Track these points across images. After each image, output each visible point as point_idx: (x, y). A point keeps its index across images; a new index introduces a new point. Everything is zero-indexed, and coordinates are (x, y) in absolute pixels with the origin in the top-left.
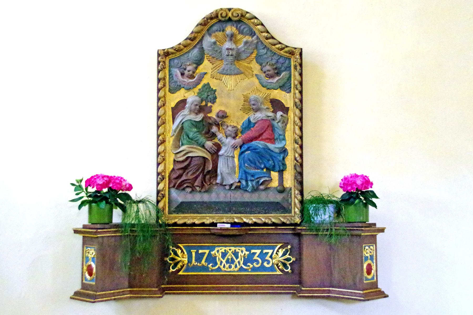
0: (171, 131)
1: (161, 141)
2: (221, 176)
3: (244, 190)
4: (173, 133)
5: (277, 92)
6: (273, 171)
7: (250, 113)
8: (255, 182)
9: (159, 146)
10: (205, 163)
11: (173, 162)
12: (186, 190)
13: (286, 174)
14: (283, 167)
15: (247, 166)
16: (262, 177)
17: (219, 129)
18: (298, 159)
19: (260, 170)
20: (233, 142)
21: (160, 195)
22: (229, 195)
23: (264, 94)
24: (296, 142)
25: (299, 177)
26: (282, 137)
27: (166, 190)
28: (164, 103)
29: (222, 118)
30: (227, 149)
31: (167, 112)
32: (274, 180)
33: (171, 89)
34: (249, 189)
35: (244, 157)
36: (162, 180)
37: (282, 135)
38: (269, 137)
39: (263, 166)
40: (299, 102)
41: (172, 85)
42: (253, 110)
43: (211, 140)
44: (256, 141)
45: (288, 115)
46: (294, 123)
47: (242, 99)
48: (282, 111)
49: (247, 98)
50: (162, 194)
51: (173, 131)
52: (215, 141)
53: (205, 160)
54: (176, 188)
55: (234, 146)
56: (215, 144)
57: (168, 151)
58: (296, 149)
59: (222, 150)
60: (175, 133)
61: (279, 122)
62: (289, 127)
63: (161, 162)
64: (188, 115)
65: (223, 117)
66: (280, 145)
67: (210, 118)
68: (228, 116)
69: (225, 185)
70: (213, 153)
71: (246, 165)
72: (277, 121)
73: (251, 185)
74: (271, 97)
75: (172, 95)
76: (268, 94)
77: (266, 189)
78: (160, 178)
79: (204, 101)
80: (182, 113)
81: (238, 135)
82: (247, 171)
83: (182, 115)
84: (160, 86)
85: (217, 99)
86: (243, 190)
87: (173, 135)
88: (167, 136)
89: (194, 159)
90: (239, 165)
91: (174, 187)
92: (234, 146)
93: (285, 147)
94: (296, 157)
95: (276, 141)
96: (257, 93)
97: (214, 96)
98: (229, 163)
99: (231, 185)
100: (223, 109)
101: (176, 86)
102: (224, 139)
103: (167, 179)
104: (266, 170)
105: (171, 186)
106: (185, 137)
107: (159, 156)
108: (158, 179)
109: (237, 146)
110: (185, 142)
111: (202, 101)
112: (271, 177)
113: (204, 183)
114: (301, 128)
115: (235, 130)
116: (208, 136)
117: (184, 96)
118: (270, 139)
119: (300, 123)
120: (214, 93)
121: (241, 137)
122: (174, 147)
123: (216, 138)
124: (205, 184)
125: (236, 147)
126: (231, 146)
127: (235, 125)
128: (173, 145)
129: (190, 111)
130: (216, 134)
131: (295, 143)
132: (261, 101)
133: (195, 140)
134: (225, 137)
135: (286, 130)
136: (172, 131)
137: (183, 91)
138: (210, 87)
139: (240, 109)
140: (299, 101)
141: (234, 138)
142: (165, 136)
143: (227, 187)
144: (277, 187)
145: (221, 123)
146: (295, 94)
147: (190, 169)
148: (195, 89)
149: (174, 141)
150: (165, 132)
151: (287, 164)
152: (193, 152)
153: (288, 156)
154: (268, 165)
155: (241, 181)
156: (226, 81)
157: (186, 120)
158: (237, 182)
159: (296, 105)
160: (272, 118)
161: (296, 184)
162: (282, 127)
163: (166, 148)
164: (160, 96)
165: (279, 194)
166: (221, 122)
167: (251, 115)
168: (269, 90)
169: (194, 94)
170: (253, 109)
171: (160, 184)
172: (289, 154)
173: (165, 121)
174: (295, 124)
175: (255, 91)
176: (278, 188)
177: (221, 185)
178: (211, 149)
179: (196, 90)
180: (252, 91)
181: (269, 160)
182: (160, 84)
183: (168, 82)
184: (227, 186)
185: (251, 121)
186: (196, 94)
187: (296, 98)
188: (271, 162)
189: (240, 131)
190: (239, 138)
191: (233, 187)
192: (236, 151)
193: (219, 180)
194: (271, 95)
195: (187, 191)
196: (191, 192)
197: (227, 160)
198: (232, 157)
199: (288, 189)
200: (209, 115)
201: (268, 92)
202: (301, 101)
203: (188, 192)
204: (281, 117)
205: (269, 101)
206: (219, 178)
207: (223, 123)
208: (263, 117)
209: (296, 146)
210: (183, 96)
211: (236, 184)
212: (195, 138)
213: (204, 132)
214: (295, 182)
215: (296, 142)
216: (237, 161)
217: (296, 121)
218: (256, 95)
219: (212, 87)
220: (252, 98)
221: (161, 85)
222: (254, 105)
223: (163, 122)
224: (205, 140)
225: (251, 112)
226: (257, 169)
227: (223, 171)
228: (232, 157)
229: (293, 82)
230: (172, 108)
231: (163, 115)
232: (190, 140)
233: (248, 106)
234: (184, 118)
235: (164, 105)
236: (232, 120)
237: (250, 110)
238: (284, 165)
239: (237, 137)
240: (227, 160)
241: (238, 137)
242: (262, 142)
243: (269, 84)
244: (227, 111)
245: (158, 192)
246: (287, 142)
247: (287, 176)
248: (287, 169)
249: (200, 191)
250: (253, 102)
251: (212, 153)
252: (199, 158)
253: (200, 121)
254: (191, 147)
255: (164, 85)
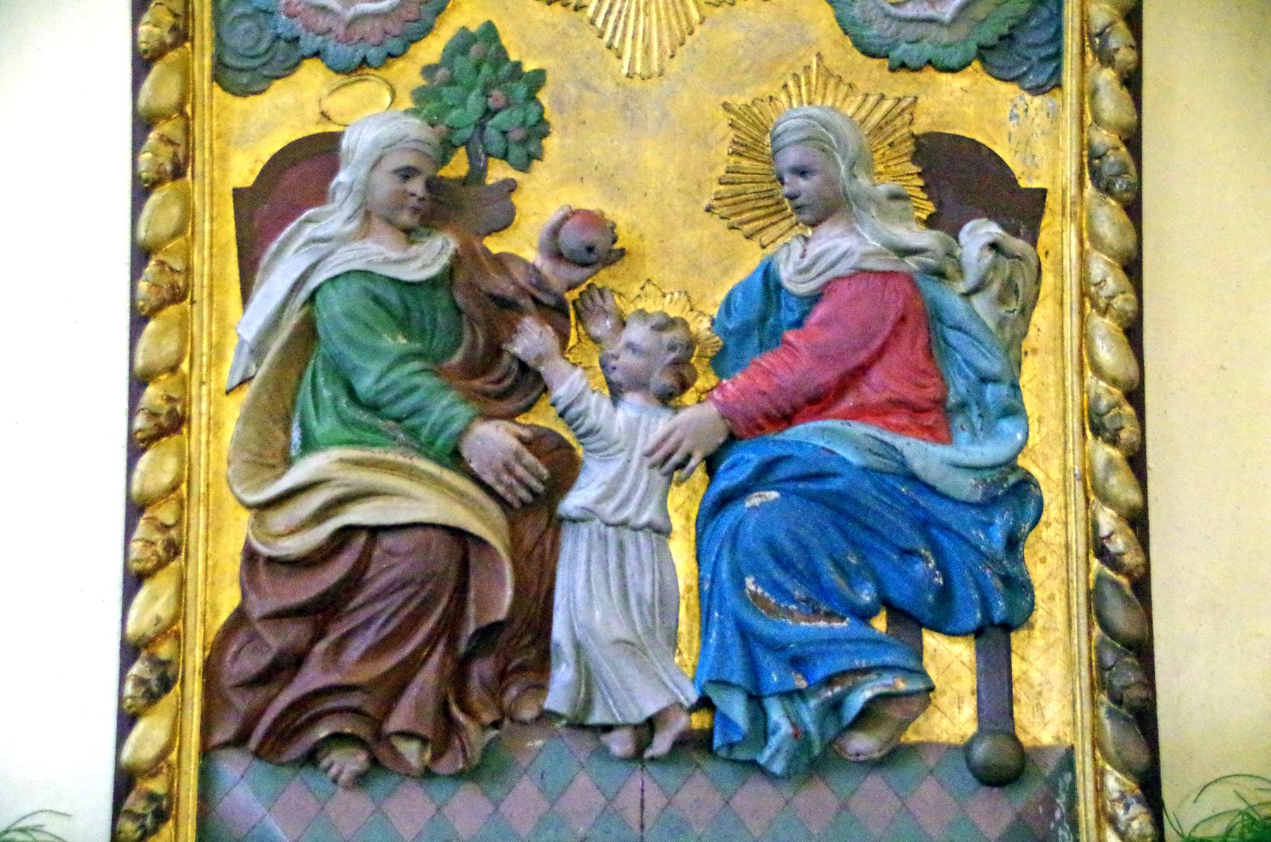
0: (231, 354)
1: (153, 415)
2: (578, 662)
3: (735, 761)
4: (246, 370)
5: (965, 91)
6: (937, 628)
7: (774, 231)
8: (813, 703)
9: (144, 450)
10: (464, 568)
11: (237, 569)
12: (325, 763)
13: (1032, 654)
14: (1010, 605)
15: (760, 591)
16: (866, 671)
17: (564, 338)
18: (1118, 544)
19: (845, 624)
20: (661, 424)
21: (134, 802)
22: (629, 798)
23: (868, 105)
24: (1097, 425)
25: (1128, 676)
26: (991, 393)
27: (184, 767)
28: (181, 156)
29: (584, 265)
30: (620, 477)
31: (198, 220)
32: (944, 692)
33: (228, 59)
34: (774, 756)
35: (734, 536)
36: (152, 698)
37: (996, 380)
38: (912, 395)
39: (866, 596)
40: (1123, 149)
41: (241, 36)
42: (798, 209)
43: (510, 417)
44: (820, 423)
45: (1039, 245)
46: (1083, 294)
47: (723, 134)
48: (993, 216)
49: (755, 133)
50: (152, 797)
51: (246, 349)
52: (541, 423)
53: (466, 553)
54: (261, 745)
55: (668, 456)
56: (538, 442)
57: (203, 490)
58: (1100, 474)
59: (582, 479)
60: (258, 366)
61: (976, 290)
62: (1044, 328)
63: (149, 565)
64: (344, 240)
65: (594, 257)
66: (989, 452)
67: (500, 261)
68: (622, 253)
69: (608, 728)
70: (523, 503)
71: (753, 588)
72: (962, 287)
73: (785, 728)
74: (922, 125)
75: (239, 104)
76: (899, 100)
77: (895, 755)
78: (141, 682)
79: (462, 150)
80: (309, 231)
81: (695, 378)
82: (761, 625)
83: (305, 244)
84: (150, 35)
85: (545, 134)
86: (726, 760)
87: (245, 381)
88: (202, 383)
89: (387, 541)
90: (700, 585)
91: (240, 740)
92: (668, 456)
93: (1021, 462)
94: (1104, 530)
95: (959, 420)
96: (824, 97)
97: (532, 119)
98: (631, 567)
99: (650, 726)
100: (588, 199)
101: (264, 46)
102: (597, 407)
103: (195, 687)
104: (888, 618)
105: (219, 737)
106: (326, 393)
107: (142, 521)
108: (129, 689)
109: (688, 457)
110: (323, 427)
111: (447, 148)
112: (922, 674)
113: (455, 710)
114: (1133, 332)
115: (672, 348)
116: (489, 387)
117: (323, 114)
118: (916, 410)
119: (1131, 296)
120: (531, 97)
121: (715, 393)
122: (246, 462)
123: (543, 404)
124: (461, 717)
125: (680, 466)
126: (649, 454)
127: (672, 315)
128: (239, 444)
129: (361, 213)
130: (542, 369)
131: (1089, 433)
132: (852, 147)
133: (397, 409)
134: (606, 392)
135: (1026, 345)
136: (239, 352)
137: (313, 76)
138: (502, 54)
139: (705, 203)
140: (1119, 143)
141: (667, 399)
142: (184, 383)
143: (620, 744)
144: (967, 748)
145: (574, 303)
146: (1089, 94)
147: (362, 616)
148: (399, 64)
149: (246, 419)
150: (187, 360)
151: (1036, 585)
152: (395, 500)
153: (1041, 524)
154: (900, 593)
155: (716, 696)
156: (609, 12)
157: (338, 271)
158: (686, 704)
159: (1096, 175)
160: (930, 261)
161: (1108, 725)
162: (1001, 324)
163: (190, 469)
164: (153, 105)
165: (984, 791)
166: (575, 294)
167: (780, 242)
168: (903, 75)
169: (388, 99)
170: (799, 201)
171: (141, 726)
172: (1052, 511)
173: (188, 286)
174: (1088, 305)
175: (808, 83)
176: (981, 752)
177: (578, 725)
178: (510, 472)
179: (408, 73)
180: (791, 83)
181: (909, 553)
182: (146, 17)
183: (207, 14)
184: (615, 735)
185: (779, 286)
186: (406, 102)
187: (1097, 121)
188: (925, 567)
189: (709, 353)
190: (699, 402)
191: (661, 744)
192: (684, 486)
193: (558, 697)
194: (918, 111)
195: (334, 770)
196: (360, 780)
197: (621, 547)
198: (658, 531)
199: (1051, 764)
200: (495, 245)
201: (903, 85)
202: (1133, 140)
203: (343, 777)
204: (989, 256)
205: (909, 147)
206: (563, 674)
207: (592, 298)
208: (865, 255)
209: (1103, 452)
210: (312, 112)
211: (681, 722)
212: (398, 398)
213: (457, 358)
214: (1103, 712)
215: (1097, 430)
216: (685, 557)
217: (1096, 285)
218: (821, 108)
219: (513, 57)
220: (790, 123)
221: (157, 31)
222: (802, 172)
223: (173, 286)
224: (463, 412)
225: (785, 224)
226: (829, 616)
227: (592, 632)
228: (658, 531)
229: (1077, 11)
230: (238, 193)
231: (174, 236)
232: (364, 417)
233: (757, 188)
234: (326, 257)
235: (178, 172)
236: (649, 280)
237: (777, 210)
238: (1018, 587)
239: (689, 397)
240: (621, 547)
241: (695, 396)
242: (859, 429)
243: (910, 31)
244: (620, 216)
245: (125, 780)
246: (1033, 427)
247: (1039, 664)
248: (1039, 616)
249: (428, 774)
250: (792, 157)
251: (517, 504)
252: (419, 534)
253: (432, 283)
254: (358, 463)
255: (182, 35)
